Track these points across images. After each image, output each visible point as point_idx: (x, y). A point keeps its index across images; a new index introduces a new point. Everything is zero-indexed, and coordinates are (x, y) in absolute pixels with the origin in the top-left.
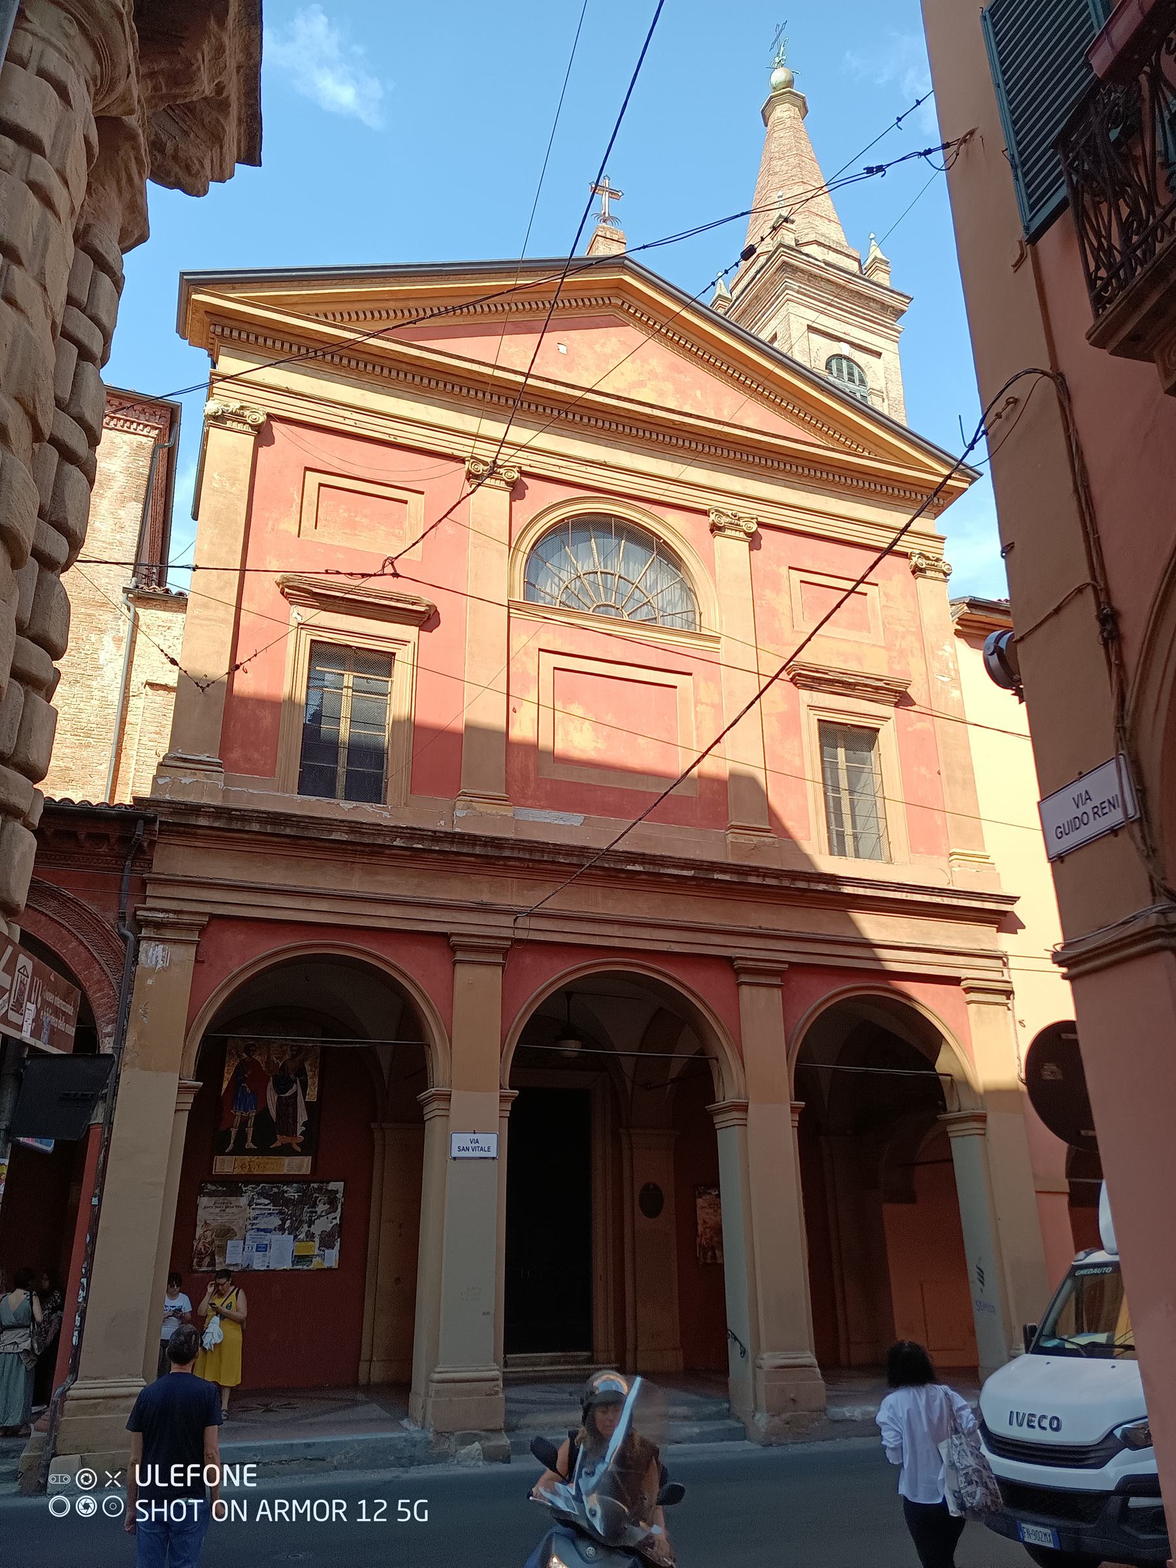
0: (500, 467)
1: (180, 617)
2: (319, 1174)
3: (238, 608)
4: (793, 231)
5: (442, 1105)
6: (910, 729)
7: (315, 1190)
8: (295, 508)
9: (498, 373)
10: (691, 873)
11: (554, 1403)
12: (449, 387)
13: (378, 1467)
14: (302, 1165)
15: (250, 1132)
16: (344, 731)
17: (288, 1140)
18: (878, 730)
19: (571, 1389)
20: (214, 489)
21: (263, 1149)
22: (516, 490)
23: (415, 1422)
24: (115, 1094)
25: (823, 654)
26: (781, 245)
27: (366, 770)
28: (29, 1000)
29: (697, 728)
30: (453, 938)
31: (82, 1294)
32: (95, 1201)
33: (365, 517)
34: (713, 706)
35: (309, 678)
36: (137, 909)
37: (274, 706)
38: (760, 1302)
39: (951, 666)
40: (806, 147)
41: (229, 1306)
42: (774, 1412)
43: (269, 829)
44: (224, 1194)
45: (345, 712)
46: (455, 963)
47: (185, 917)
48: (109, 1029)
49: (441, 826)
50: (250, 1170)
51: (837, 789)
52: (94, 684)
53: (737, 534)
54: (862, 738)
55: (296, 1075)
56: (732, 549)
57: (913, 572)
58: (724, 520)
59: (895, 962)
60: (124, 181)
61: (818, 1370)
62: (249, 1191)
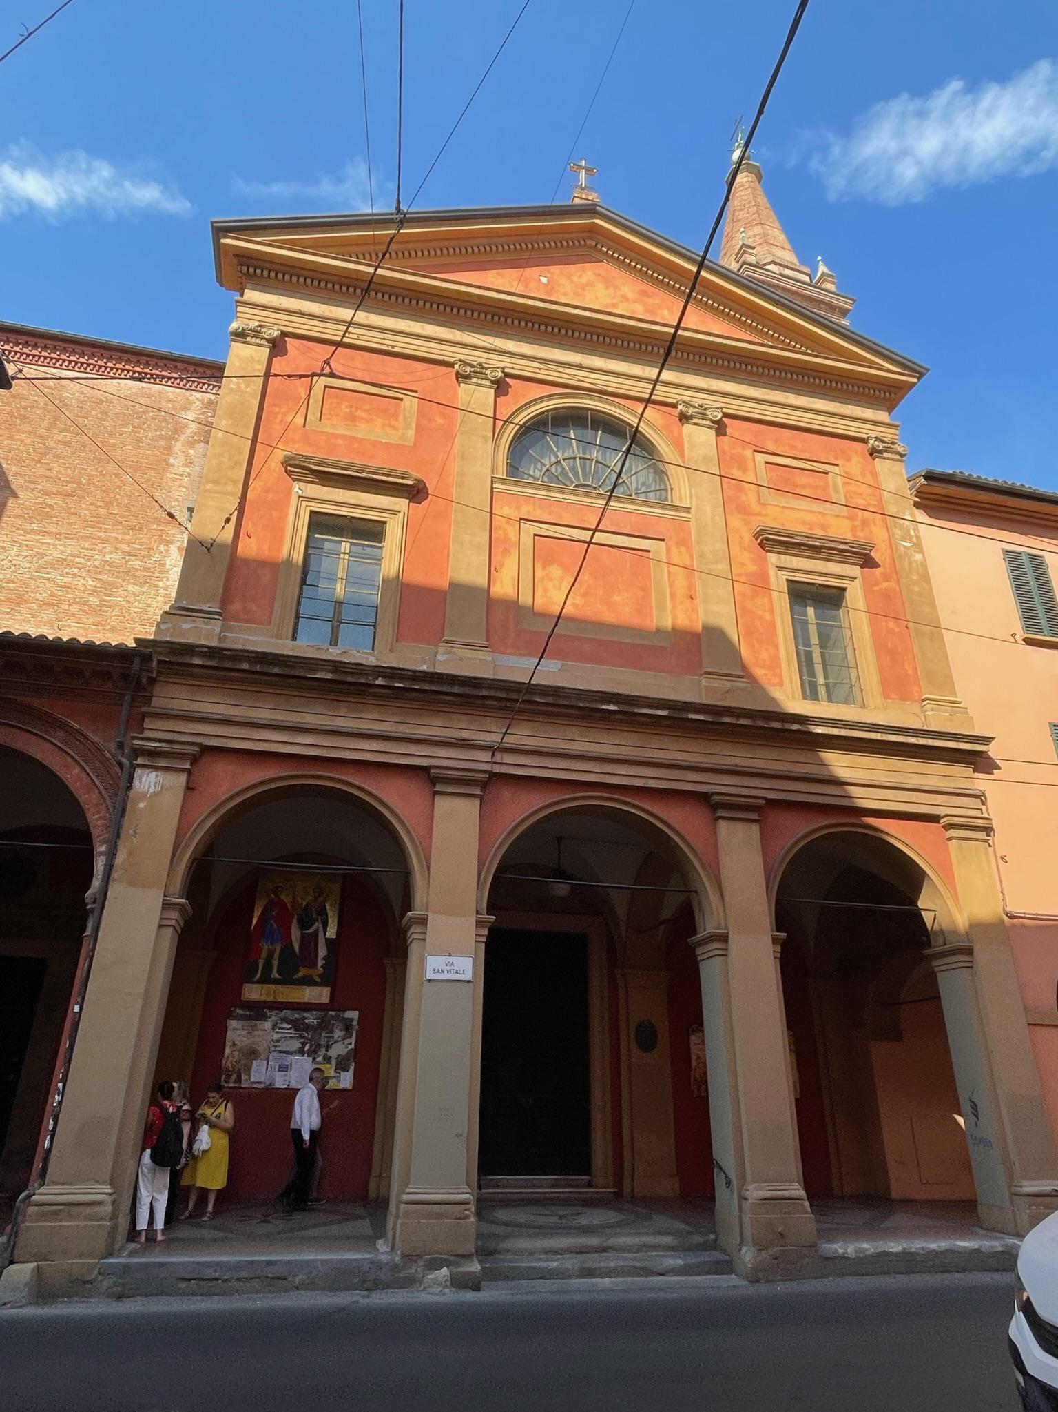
2: (336, 1003)
4: (755, 255)
5: (419, 929)
6: (875, 588)
10: (665, 713)
11: (539, 1228)
13: (340, 1289)
14: (322, 994)
15: (275, 963)
17: (310, 972)
18: (844, 589)
19: (561, 1213)
21: (287, 979)
22: (501, 387)
26: (744, 263)
29: (671, 587)
31: (57, 1098)
32: (77, 1009)
33: (365, 411)
37: (275, 567)
38: (745, 1131)
40: (762, 200)
41: (218, 1117)
43: (258, 668)
44: (249, 1018)
46: (435, 793)
51: (807, 644)
52: (161, 584)
54: (828, 598)
55: (318, 914)
56: (700, 437)
57: (871, 455)
58: (691, 410)
59: (865, 799)
61: (807, 1203)
62: (273, 1016)
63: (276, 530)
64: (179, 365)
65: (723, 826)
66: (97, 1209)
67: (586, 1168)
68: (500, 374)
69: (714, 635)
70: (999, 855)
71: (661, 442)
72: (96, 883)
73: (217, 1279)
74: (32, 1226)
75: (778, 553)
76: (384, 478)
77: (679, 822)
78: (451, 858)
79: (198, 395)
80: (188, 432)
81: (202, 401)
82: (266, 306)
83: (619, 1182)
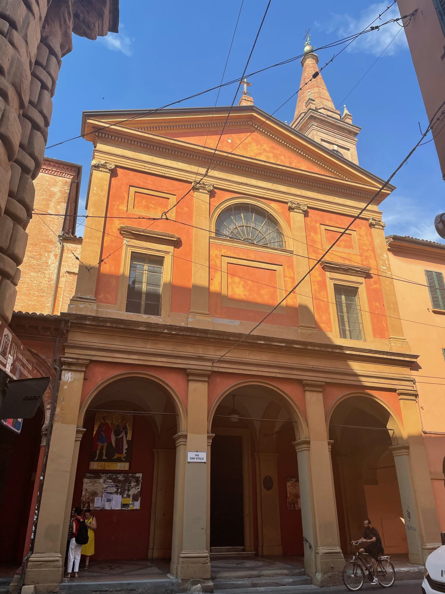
0: (206, 185)
1: (79, 246)
2: (132, 470)
3: (104, 233)
4: (314, 104)
5: (183, 440)
6: (371, 288)
7: (131, 477)
8: (126, 201)
9: (205, 149)
10: (284, 345)
11: (230, 568)
12: (186, 155)
14: (125, 466)
15: (104, 452)
16: (144, 288)
18: (358, 288)
20: (94, 193)
21: (110, 459)
22: (212, 194)
23: (173, 575)
24: (51, 433)
25: (338, 255)
26: (310, 109)
27: (153, 303)
28: (10, 353)
30: (188, 370)
31: (36, 517)
32: (42, 478)
33: (153, 204)
34: (291, 278)
35: (130, 267)
36: (61, 357)
37: (118, 278)
39: (387, 262)
41: (90, 523)
42: (324, 573)
43: (114, 325)
44: (94, 478)
45: (145, 280)
46: (188, 381)
47: (80, 361)
48: (49, 407)
49: (183, 324)
50: (104, 467)
51: (342, 312)
52: (47, 272)
53: (299, 211)
56: (297, 217)
58: (294, 206)
59: (367, 382)
60: (62, 22)
61: (342, 554)
62: (104, 476)
63: (117, 262)
64: (52, 163)
65: (308, 394)
66: (57, 563)
67: (242, 543)
68: (212, 188)
69: (304, 309)
70: (420, 407)
71: (278, 217)
72: (47, 422)
73: (107, 591)
74: (31, 571)
75: (330, 272)
76: (164, 237)
77: (290, 392)
78: (196, 408)
79: (61, 178)
80: (57, 197)
81: (62, 181)
82: (108, 153)
83: (256, 549)
